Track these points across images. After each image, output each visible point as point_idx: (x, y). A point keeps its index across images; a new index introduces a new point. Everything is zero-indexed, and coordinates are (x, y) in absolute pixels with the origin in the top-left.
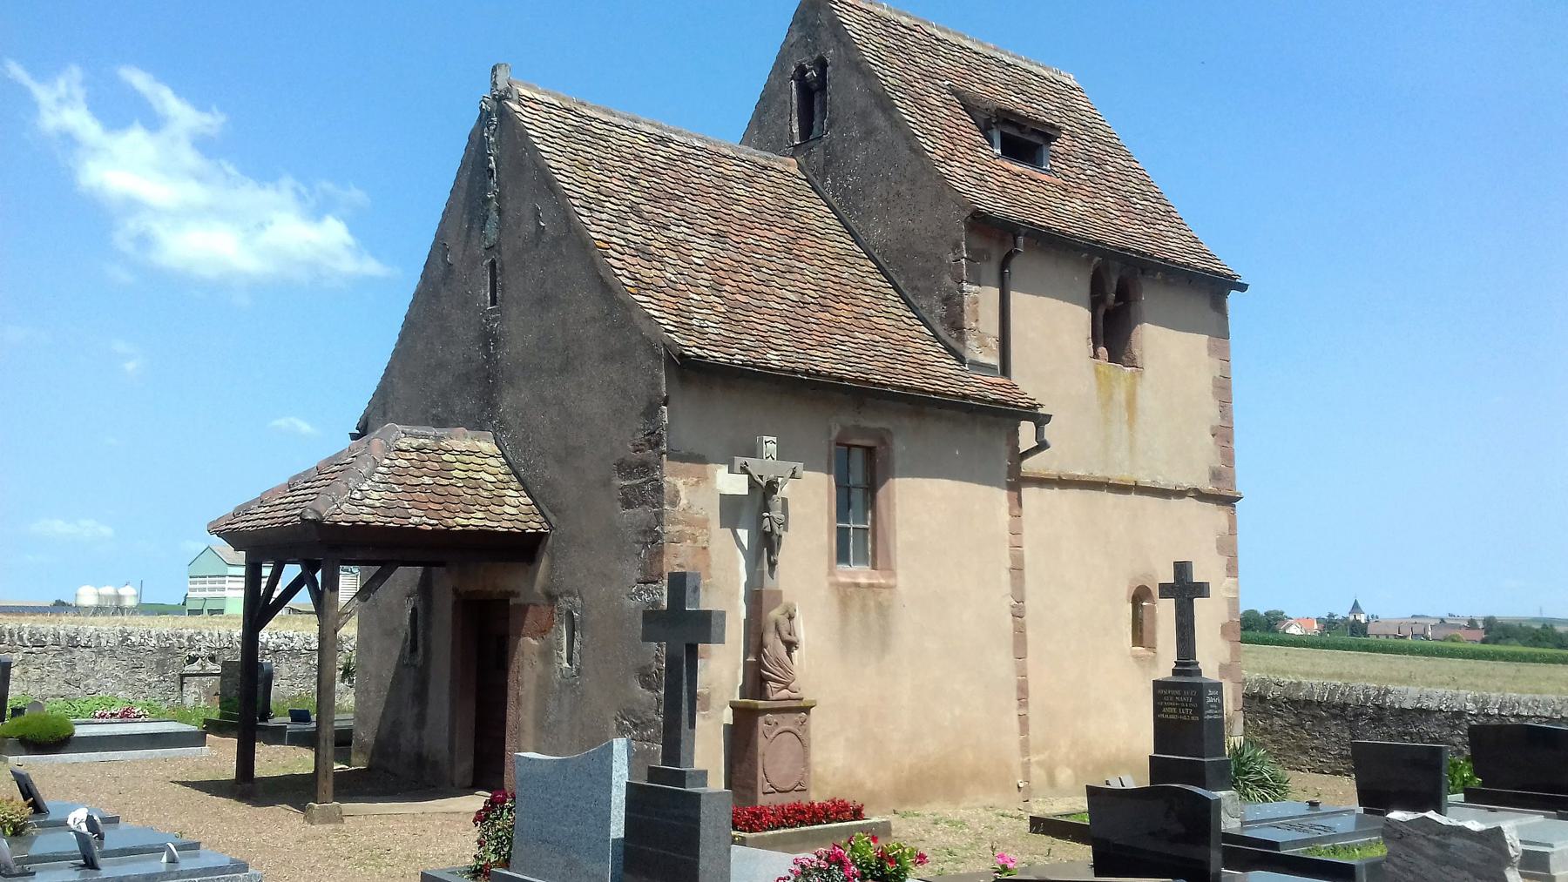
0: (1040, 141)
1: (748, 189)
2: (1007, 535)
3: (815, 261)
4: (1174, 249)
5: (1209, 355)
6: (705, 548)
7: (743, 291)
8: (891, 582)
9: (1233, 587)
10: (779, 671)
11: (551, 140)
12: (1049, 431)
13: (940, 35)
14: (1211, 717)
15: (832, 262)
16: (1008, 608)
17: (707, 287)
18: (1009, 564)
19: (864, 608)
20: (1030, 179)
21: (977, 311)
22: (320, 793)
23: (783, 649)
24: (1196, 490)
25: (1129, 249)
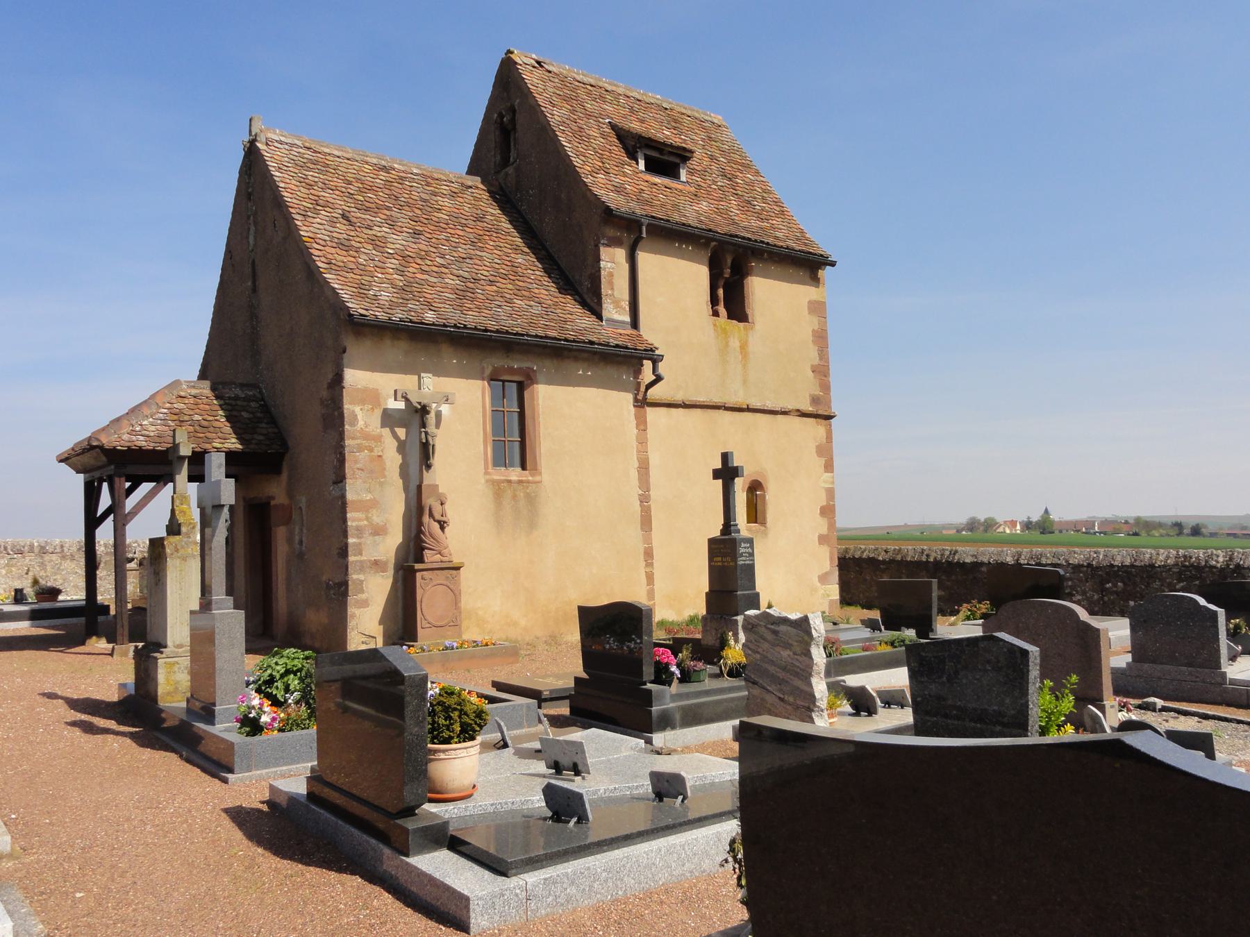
0: (677, 161)
1: (451, 202)
2: (635, 444)
3: (495, 251)
4: (781, 236)
5: (809, 313)
6: (380, 456)
7: (423, 272)
8: (537, 478)
9: (831, 480)
10: (433, 542)
11: (286, 168)
12: (662, 368)
13: (609, 88)
14: (743, 562)
15: (510, 251)
16: (636, 497)
17: (393, 269)
18: (636, 465)
19: (514, 497)
20: (666, 187)
21: (613, 283)
22: (119, 638)
23: (437, 525)
24: (798, 410)
25: (737, 236)
